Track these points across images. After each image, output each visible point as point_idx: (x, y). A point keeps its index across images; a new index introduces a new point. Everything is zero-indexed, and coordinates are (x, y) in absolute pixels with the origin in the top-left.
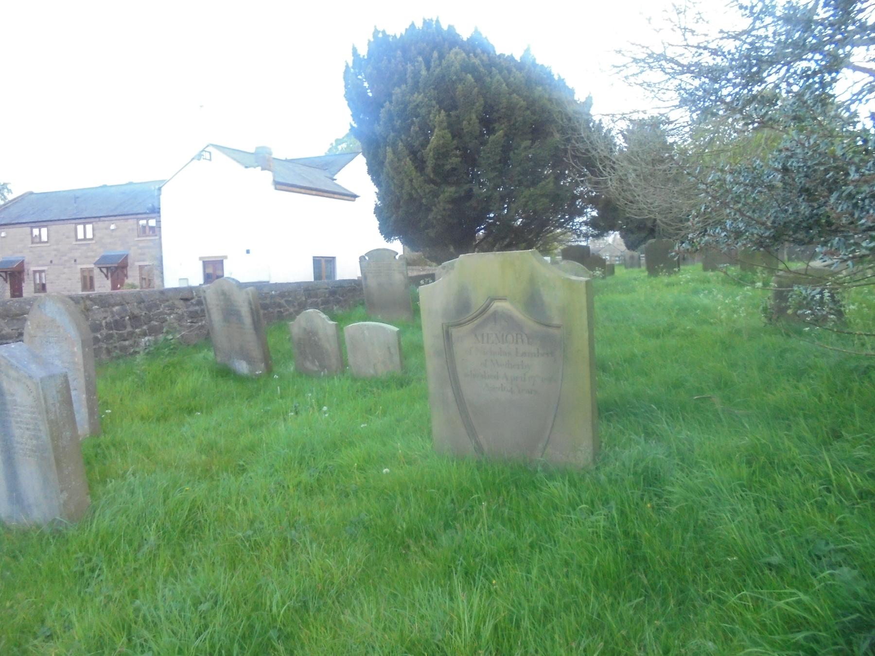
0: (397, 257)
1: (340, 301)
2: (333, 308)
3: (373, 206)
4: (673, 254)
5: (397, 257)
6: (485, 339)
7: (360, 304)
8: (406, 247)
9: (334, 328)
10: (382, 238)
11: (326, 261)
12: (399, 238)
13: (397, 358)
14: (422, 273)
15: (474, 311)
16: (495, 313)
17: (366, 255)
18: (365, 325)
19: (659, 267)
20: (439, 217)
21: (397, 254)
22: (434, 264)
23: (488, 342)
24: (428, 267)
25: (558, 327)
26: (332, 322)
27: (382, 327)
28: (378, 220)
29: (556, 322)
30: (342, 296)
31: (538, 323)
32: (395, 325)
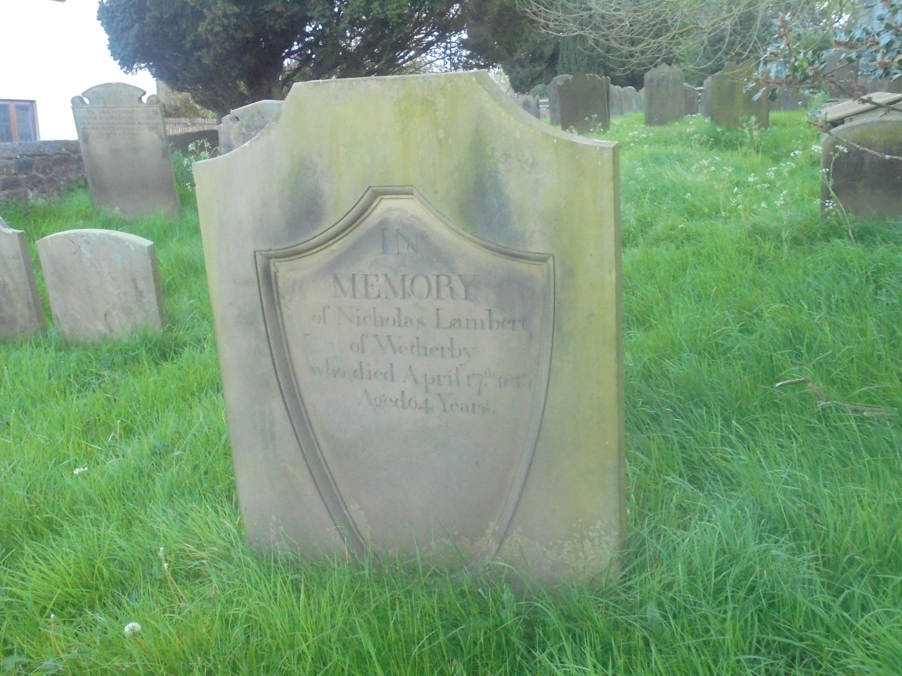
0: (144, 99)
1: (40, 181)
2: (26, 195)
3: (96, 7)
4: (751, 85)
5: (144, 99)
6: (360, 286)
7: (79, 187)
8: (163, 84)
9: (16, 238)
10: (115, 65)
11: (17, 107)
12: (149, 67)
13: (151, 299)
14: (191, 130)
15: (332, 220)
16: (383, 227)
17: (83, 94)
18: (82, 236)
19: (591, 118)
20: (217, 29)
21: (144, 93)
22: (210, 113)
23: (367, 296)
24: (200, 120)
25: (542, 259)
26: (10, 231)
27: (117, 240)
28: (108, 32)
29: (537, 247)
30: (44, 172)
31: (488, 248)
32: (146, 236)
